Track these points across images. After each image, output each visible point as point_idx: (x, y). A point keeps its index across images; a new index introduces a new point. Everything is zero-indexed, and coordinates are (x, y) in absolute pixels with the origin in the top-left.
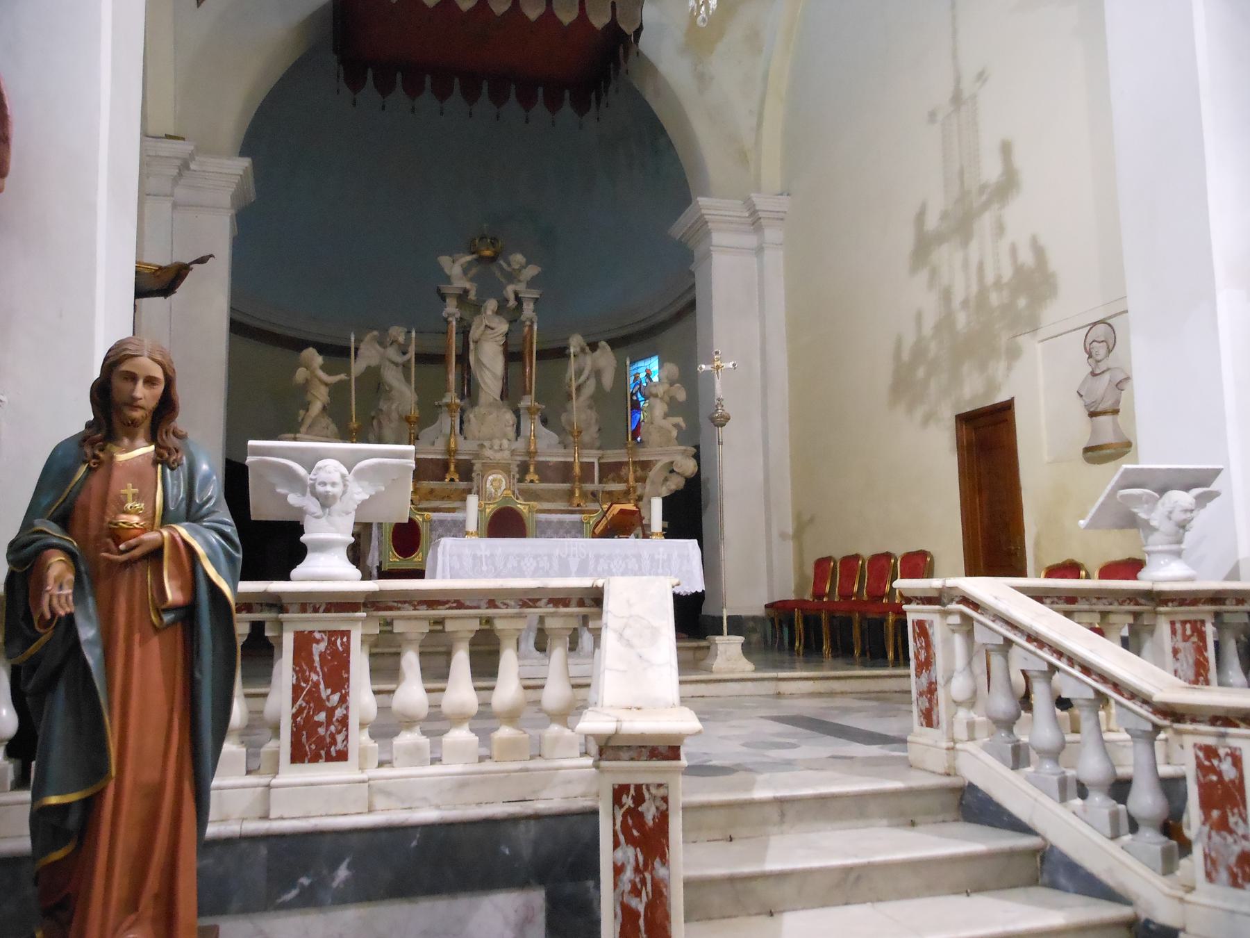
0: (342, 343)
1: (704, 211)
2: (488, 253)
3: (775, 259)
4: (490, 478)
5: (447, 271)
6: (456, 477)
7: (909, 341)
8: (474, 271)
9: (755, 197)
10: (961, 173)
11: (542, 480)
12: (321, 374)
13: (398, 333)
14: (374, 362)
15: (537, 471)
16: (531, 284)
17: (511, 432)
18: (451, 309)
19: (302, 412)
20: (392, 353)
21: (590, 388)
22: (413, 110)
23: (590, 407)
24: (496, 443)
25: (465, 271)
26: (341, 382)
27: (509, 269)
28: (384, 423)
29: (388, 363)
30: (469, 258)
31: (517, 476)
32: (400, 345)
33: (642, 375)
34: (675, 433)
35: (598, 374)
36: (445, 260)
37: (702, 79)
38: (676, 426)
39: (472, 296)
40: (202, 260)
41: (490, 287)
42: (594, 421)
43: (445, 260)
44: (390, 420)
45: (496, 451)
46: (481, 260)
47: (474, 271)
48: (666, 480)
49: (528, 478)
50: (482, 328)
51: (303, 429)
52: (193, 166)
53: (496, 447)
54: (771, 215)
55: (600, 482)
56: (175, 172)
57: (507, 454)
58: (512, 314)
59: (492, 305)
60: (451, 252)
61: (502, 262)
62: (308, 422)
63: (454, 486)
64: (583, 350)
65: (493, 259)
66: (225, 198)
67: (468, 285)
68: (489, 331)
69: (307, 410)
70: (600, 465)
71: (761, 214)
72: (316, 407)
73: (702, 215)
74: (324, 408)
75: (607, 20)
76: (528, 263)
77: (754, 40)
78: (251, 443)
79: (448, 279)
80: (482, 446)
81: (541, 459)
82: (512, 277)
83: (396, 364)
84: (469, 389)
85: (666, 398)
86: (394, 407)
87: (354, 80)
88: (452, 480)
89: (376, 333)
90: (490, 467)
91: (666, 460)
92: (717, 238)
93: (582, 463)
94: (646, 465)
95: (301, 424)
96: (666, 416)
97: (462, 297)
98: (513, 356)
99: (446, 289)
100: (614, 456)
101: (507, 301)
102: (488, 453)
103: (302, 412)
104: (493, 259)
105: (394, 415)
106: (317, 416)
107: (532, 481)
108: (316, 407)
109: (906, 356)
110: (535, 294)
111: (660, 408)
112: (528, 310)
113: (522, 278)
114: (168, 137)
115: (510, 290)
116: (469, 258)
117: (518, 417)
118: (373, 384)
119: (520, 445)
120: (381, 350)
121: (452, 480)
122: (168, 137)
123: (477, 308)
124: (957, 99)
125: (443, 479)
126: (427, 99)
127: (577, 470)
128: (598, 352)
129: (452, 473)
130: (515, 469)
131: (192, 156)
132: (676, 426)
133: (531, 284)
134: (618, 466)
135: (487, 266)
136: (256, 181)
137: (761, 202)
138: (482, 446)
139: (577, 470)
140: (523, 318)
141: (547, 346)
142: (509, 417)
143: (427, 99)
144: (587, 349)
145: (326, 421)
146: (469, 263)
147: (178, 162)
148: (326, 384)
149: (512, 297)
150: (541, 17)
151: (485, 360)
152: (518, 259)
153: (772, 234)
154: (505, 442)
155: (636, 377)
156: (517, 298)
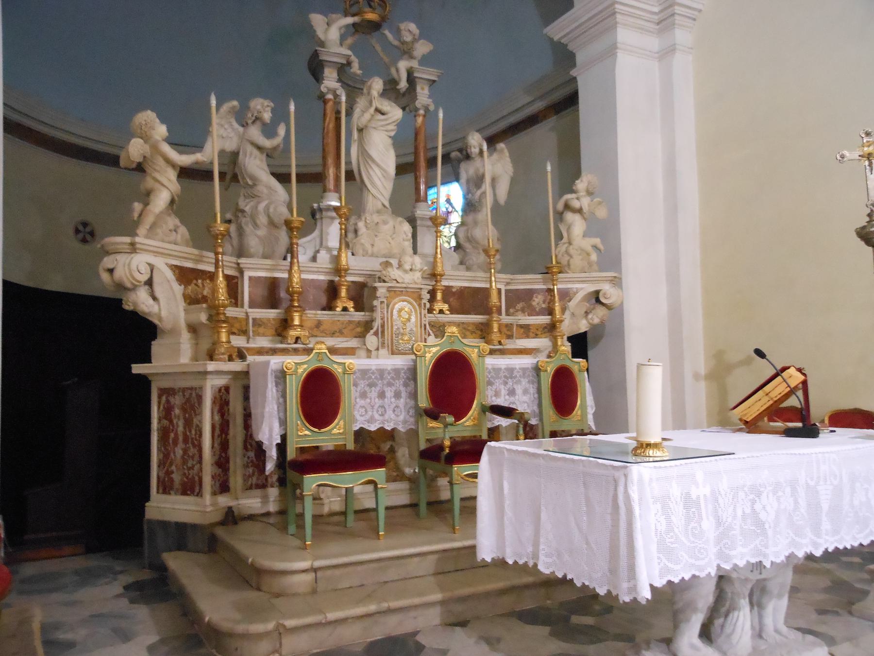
2: (371, 16)
3: (684, 65)
5: (320, 33)
6: (350, 305)
8: (350, 41)
12: (166, 149)
13: (263, 107)
14: (230, 146)
19: (137, 206)
20: (255, 133)
28: (248, 229)
29: (249, 148)
32: (264, 124)
36: (317, 20)
38: (595, 247)
43: (317, 20)
44: (256, 225)
45: (406, 271)
47: (350, 41)
50: (372, 110)
51: (142, 230)
53: (407, 267)
58: (402, 94)
59: (377, 85)
60: (328, 10)
61: (387, 32)
62: (149, 220)
65: (375, 26)
69: (146, 204)
71: (678, 10)
72: (161, 200)
80: (387, 264)
82: (406, 52)
83: (259, 148)
86: (261, 207)
88: (345, 309)
89: (235, 103)
94: (566, 295)
95: (136, 224)
96: (585, 235)
97: (343, 69)
102: (394, 273)
103: (137, 206)
104: (375, 26)
105: (263, 220)
108: (161, 200)
110: (430, 74)
112: (423, 96)
116: (350, 20)
120: (241, 129)
121: (345, 309)
129: (344, 301)
132: (595, 247)
133: (425, 61)
134: (529, 294)
140: (418, 104)
141: (305, 170)
142: (407, 228)
145: (172, 221)
148: (173, 165)
149: (404, 76)
152: (409, 29)
153: (682, 36)
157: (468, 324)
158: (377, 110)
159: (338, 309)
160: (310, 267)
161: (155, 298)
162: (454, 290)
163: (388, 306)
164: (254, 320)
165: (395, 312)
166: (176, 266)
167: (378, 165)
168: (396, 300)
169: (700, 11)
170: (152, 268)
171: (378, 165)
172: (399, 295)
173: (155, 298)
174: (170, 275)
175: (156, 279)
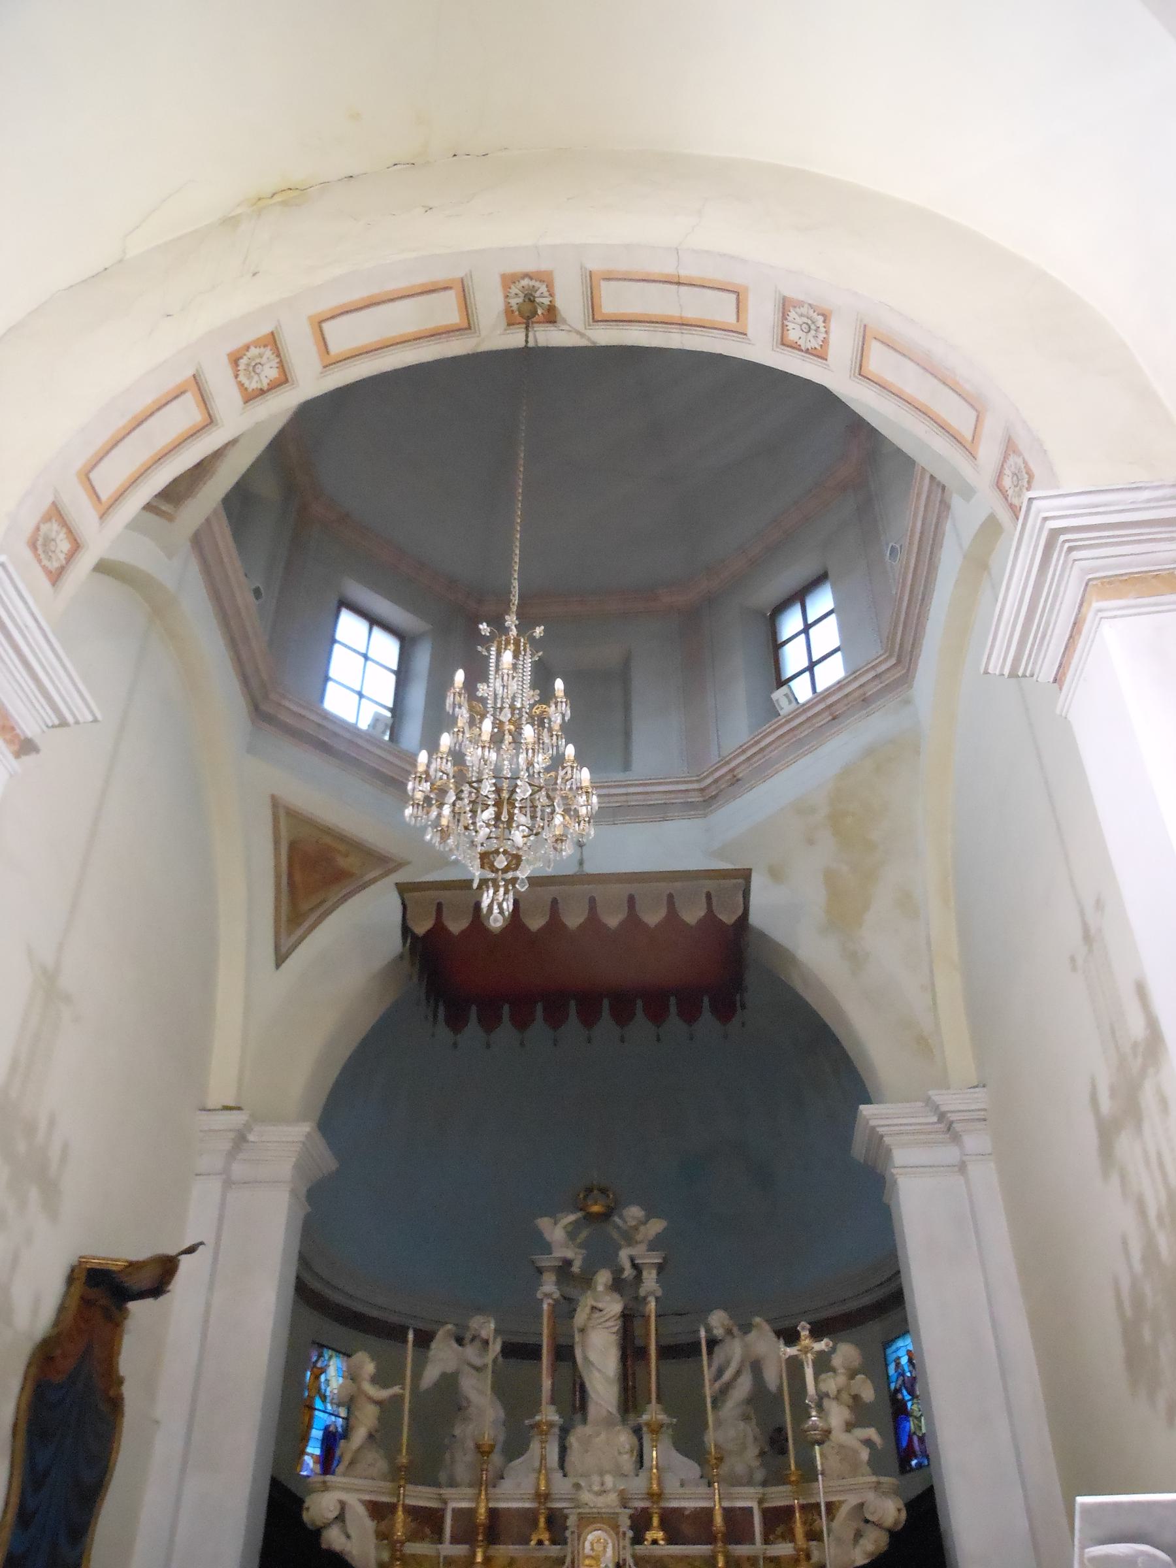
0: (532, 1340)
1: (872, 1123)
2: (596, 1209)
4: (590, 1537)
5: (547, 1236)
6: (545, 1536)
7: (1125, 1283)
8: (584, 1234)
9: (937, 1096)
10: (1113, 1032)
11: (670, 1541)
14: (450, 1368)
15: (663, 1525)
16: (653, 1246)
17: (627, 1462)
18: (549, 1287)
21: (744, 1386)
22: (455, 1045)
23: (746, 1418)
24: (596, 1479)
25: (572, 1233)
26: (395, 1396)
27: (625, 1227)
29: (467, 1369)
30: (572, 1218)
31: (630, 1534)
33: (904, 1360)
34: (865, 1454)
35: (756, 1367)
36: (544, 1223)
37: (855, 959)
38: (868, 1442)
39: (576, 1269)
40: (191, 1250)
41: (601, 1254)
42: (750, 1439)
43: (544, 1223)
46: (590, 1218)
47: (584, 1234)
48: (858, 1535)
49: (650, 1535)
50: (588, 1310)
52: (251, 1137)
54: (967, 1116)
55: (766, 1541)
56: (227, 1146)
57: (612, 1499)
59: (603, 1278)
60: (553, 1213)
63: (541, 1554)
64: (729, 1332)
65: (606, 1216)
66: (285, 1169)
67: (569, 1254)
68: (597, 1314)
70: (765, 1512)
71: (953, 1117)
73: (873, 1128)
74: (370, 1436)
75: (702, 913)
76: (648, 1218)
77: (908, 905)
78: (1080, 1500)
79: (547, 1248)
81: (674, 1504)
82: (629, 1238)
84: (575, 1400)
85: (845, 1396)
87: (456, 1022)
88: (540, 1543)
90: (589, 1520)
91: (852, 1500)
92: (900, 1157)
93: (724, 1509)
96: (849, 1427)
98: (631, 1351)
99: (544, 1261)
100: (780, 1496)
101: (622, 1270)
102: (586, 1497)
106: (360, 1449)
107: (655, 1542)
109: (1129, 1313)
111: (837, 1416)
112: (650, 1280)
113: (639, 1237)
114: (227, 1108)
115: (624, 1255)
116: (572, 1218)
117: (640, 1439)
118: (445, 1402)
119: (638, 1485)
122: (227, 1108)
123: (586, 1281)
124: (1088, 938)
125: (527, 1541)
126: (506, 1031)
127: (718, 1520)
128: (752, 1336)
130: (625, 1522)
131: (248, 1127)
132: (868, 1442)
135: (598, 1222)
136: (331, 1145)
137: (949, 1101)
138: (577, 1486)
139: (718, 1520)
142: (624, 1439)
143: (506, 1031)
144: (735, 1330)
146: (576, 1221)
147: (232, 1135)
149: (627, 1265)
150: (622, 924)
151: (593, 1356)
152: (634, 1212)
153: (976, 1142)
154: (609, 1480)
155: (898, 1365)
156: (635, 1266)
157: (694, 1558)
158: (593, 1308)
159: (533, 1543)
160: (515, 1494)
161: (348, 1537)
162: (687, 1513)
163: (579, 1537)
164: (445, 1557)
165: (587, 1544)
166: (370, 1502)
167: (599, 1371)
168: (590, 1528)
169: (985, 1110)
170: (343, 1505)
171: (599, 1371)
172: (592, 1523)
173: (348, 1537)
174: (361, 1510)
175: (348, 1516)
